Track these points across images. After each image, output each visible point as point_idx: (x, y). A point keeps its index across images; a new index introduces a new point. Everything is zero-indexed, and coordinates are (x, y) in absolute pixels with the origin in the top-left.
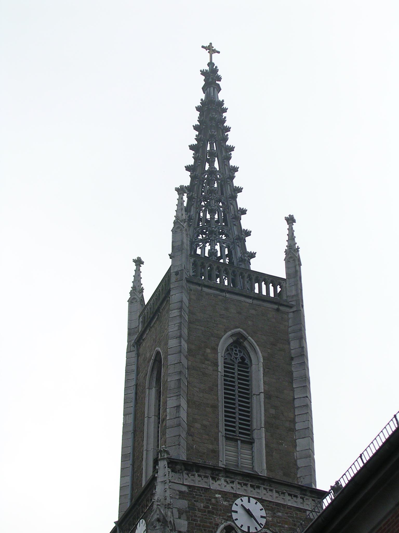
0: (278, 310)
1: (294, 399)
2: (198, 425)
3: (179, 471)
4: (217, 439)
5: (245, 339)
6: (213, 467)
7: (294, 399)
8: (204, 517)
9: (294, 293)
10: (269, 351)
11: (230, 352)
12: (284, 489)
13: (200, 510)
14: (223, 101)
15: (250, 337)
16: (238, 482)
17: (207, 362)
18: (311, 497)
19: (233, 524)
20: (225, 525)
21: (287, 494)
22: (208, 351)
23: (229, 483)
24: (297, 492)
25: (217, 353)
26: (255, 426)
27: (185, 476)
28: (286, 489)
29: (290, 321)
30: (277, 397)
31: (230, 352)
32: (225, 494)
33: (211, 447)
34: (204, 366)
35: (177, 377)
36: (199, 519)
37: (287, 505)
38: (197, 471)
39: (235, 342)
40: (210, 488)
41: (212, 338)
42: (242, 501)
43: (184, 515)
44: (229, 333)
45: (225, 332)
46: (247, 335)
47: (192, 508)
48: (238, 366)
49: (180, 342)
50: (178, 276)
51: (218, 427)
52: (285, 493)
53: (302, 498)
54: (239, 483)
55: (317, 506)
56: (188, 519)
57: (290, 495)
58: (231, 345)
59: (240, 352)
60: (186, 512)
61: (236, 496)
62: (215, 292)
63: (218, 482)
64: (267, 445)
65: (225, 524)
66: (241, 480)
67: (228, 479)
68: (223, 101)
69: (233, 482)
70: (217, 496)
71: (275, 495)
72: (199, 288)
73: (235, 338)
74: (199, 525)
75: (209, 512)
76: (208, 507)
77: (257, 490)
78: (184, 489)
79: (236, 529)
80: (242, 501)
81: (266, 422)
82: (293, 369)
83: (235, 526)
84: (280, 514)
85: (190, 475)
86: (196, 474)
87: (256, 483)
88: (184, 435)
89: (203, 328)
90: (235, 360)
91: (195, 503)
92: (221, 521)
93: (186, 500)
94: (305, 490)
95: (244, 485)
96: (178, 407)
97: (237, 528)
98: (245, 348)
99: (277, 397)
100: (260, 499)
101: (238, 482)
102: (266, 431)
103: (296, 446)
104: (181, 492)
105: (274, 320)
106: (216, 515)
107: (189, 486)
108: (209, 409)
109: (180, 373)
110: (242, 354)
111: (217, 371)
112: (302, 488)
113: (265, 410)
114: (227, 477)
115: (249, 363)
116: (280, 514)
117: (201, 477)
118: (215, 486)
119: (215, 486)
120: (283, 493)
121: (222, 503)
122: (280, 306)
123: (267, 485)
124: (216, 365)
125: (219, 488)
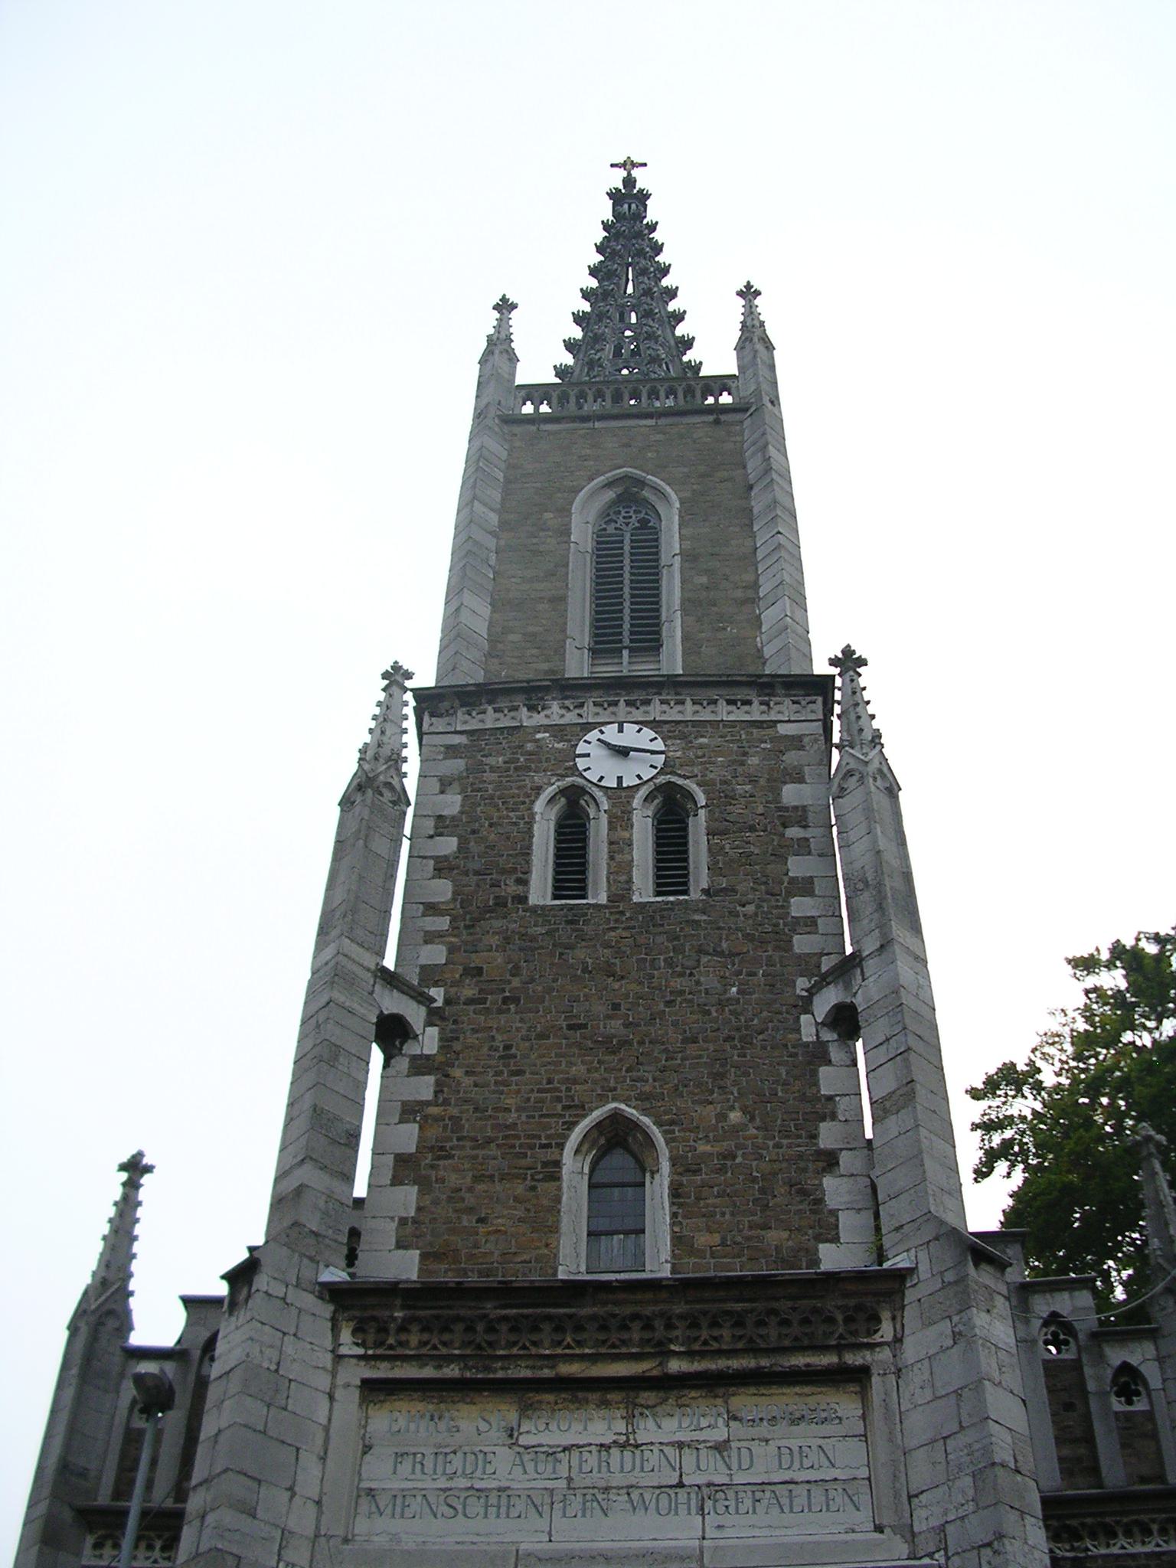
0: (717, 422)
3: (447, 711)
5: (642, 483)
6: (525, 684)
8: (504, 780)
13: (493, 769)
15: (649, 477)
16: (594, 702)
18: (786, 696)
19: (580, 780)
20: (558, 787)
21: (722, 703)
23: (571, 708)
24: (752, 694)
26: (664, 617)
28: (720, 693)
32: (558, 731)
36: (490, 787)
37: (722, 721)
38: (489, 703)
39: (619, 500)
40: (522, 726)
42: (651, 766)
43: (456, 786)
46: (644, 475)
47: (475, 769)
52: (717, 700)
54: (595, 704)
57: (730, 702)
62: (568, 425)
65: (559, 783)
66: (601, 697)
67: (567, 703)
72: (533, 428)
73: (620, 490)
78: (457, 740)
79: (588, 789)
80: (651, 766)
83: (585, 783)
85: (474, 713)
86: (490, 708)
90: (624, 527)
91: (484, 759)
92: (550, 779)
93: (461, 758)
95: (609, 705)
97: (590, 785)
98: (646, 500)
100: (651, 722)
101: (594, 702)
106: (535, 772)
112: (759, 680)
113: (683, 582)
114: (566, 698)
117: (503, 712)
121: (550, 746)
122: (721, 414)
123: (668, 694)
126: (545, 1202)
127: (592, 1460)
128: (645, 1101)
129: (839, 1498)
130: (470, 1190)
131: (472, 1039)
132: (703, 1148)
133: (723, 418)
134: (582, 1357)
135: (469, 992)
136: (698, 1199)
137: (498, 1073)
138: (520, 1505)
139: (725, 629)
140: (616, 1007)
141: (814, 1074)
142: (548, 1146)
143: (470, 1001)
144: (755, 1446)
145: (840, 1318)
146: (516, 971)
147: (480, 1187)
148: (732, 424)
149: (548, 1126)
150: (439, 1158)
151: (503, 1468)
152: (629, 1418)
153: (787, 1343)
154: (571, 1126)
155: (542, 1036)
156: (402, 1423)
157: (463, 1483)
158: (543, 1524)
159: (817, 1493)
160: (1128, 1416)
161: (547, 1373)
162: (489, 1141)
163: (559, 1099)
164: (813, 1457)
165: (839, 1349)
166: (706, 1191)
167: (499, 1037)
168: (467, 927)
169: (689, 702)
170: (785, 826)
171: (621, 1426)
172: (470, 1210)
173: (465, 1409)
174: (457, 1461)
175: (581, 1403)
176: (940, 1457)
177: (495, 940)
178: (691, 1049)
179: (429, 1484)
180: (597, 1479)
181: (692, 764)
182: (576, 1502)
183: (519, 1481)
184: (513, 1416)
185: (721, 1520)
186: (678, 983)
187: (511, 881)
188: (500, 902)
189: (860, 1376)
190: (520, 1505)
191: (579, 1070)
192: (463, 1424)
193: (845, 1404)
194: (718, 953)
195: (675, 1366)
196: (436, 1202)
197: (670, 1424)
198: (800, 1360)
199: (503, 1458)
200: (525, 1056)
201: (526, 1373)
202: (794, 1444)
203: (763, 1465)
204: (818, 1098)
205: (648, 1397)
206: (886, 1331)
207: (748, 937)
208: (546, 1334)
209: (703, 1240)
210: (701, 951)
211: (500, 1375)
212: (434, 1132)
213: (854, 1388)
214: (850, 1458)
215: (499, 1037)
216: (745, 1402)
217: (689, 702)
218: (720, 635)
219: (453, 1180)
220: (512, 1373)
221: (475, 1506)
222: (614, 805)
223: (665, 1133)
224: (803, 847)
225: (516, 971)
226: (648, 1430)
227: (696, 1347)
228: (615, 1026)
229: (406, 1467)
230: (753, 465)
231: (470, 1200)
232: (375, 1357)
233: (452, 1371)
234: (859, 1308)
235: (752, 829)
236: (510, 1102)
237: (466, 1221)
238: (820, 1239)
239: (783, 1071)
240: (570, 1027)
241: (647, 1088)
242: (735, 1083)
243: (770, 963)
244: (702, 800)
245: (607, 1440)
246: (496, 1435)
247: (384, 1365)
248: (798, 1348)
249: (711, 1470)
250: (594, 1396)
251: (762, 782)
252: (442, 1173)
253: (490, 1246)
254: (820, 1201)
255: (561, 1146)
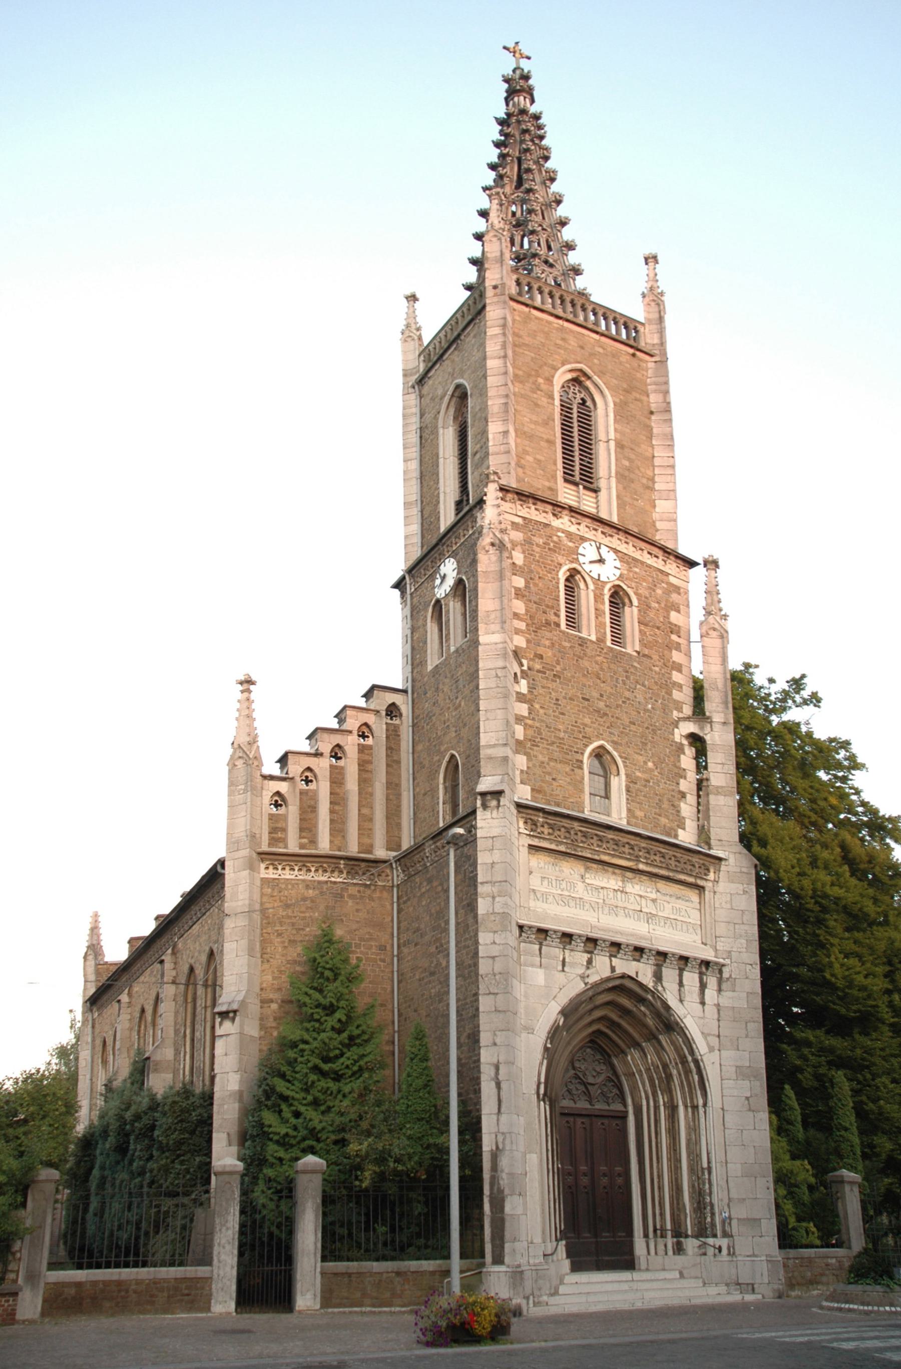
0: (634, 355)
1: (654, 457)
2: (530, 458)
4: (554, 477)
7: (654, 457)
9: (656, 341)
10: (622, 397)
11: (566, 389)
12: (643, 545)
13: (538, 545)
14: (529, 72)
17: (539, 392)
21: (645, 552)
22: (540, 380)
24: (660, 553)
25: (552, 385)
27: (519, 507)
29: (650, 371)
30: (632, 449)
31: (566, 389)
32: (569, 535)
33: (547, 484)
34: (535, 396)
35: (503, 401)
38: (534, 504)
41: (546, 368)
44: (569, 367)
45: (563, 364)
48: (578, 408)
49: (506, 363)
50: (498, 291)
51: (555, 464)
53: (665, 561)
55: (494, 898)
56: (524, 552)
57: (649, 553)
58: (568, 381)
59: (580, 392)
60: (521, 544)
61: (583, 539)
63: (560, 520)
64: (618, 497)
67: (573, 520)
68: (529, 72)
69: (579, 524)
70: (560, 534)
71: (632, 549)
74: (538, 561)
75: (549, 549)
76: (549, 544)
77: (609, 538)
81: (617, 473)
82: (653, 424)
84: (637, 570)
87: (607, 530)
88: (513, 464)
89: (533, 355)
94: (669, 553)
96: (506, 433)
98: (587, 389)
99: (632, 449)
102: (618, 481)
103: (654, 507)
104: (513, 523)
105: (628, 366)
107: (524, 518)
108: (543, 444)
109: (507, 396)
110: (582, 396)
111: (553, 404)
113: (616, 460)
114: (572, 517)
115: (591, 406)
116: (637, 570)
118: (556, 523)
119: (556, 523)
120: (642, 550)
124: (552, 397)
125: (561, 526)
126: (578, 778)
127: (611, 895)
128: (614, 743)
129: (691, 930)
130: (548, 764)
131: (541, 691)
132: (638, 774)
133: (638, 353)
134: (609, 854)
135: (538, 666)
136: (637, 795)
137: (554, 711)
138: (587, 906)
139: (637, 500)
140: (602, 695)
141: (679, 756)
142: (577, 752)
143: (539, 671)
144: (665, 903)
145: (697, 866)
146: (558, 663)
147: (552, 764)
148: (641, 360)
149: (577, 744)
150: (533, 745)
151: (580, 890)
152: (623, 881)
153: (679, 869)
154: (586, 746)
155: (571, 699)
156: (542, 865)
157: (567, 893)
158: (596, 915)
159: (684, 926)
160: (363, 746)
161: (596, 857)
162: (553, 743)
163: (580, 732)
164: (683, 913)
165: (696, 877)
166: (639, 793)
167: (553, 694)
168: (534, 631)
169: (631, 544)
170: (672, 632)
171: (620, 884)
172: (549, 774)
173: (565, 863)
174: (564, 883)
175: (607, 871)
176: (732, 929)
177: (547, 643)
178: (633, 727)
179: (555, 892)
180: (613, 902)
181: (631, 580)
182: (606, 910)
183: (587, 897)
184: (582, 870)
185: (655, 927)
186: (627, 694)
187: (552, 613)
188: (548, 623)
189: (701, 889)
190: (587, 906)
191: (587, 721)
192: (565, 870)
193: (693, 896)
194: (643, 685)
195: (641, 867)
196: (534, 765)
197: (637, 887)
198: (682, 877)
199: (580, 886)
200: (565, 707)
201: (589, 856)
202: (678, 906)
203: (667, 911)
204: (680, 768)
205: (629, 874)
206: (711, 876)
207: (656, 683)
208: (595, 841)
209: (639, 814)
210: (637, 682)
211: (580, 854)
212: (530, 732)
213: (697, 891)
214: (694, 917)
215: (553, 694)
216: (661, 885)
217: (631, 544)
218: (635, 502)
219: (540, 757)
220: (584, 854)
221: (572, 904)
222: (596, 588)
223: (624, 762)
224: (678, 647)
225: (558, 663)
226: (629, 888)
227: (649, 862)
228: (601, 705)
229: (545, 882)
230: (654, 399)
231: (548, 769)
232: (533, 836)
233: (562, 848)
234: (703, 864)
235: (658, 628)
236: (561, 727)
237: (548, 778)
238: (678, 826)
239: (668, 750)
240: (583, 698)
241: (615, 739)
242: (650, 750)
243: (664, 699)
244: (635, 602)
245: (616, 888)
246: (577, 877)
247: (536, 840)
248: (682, 872)
249: (650, 908)
250: (610, 869)
251: (663, 605)
252: (535, 753)
253: (558, 792)
254: (679, 811)
255: (582, 754)
